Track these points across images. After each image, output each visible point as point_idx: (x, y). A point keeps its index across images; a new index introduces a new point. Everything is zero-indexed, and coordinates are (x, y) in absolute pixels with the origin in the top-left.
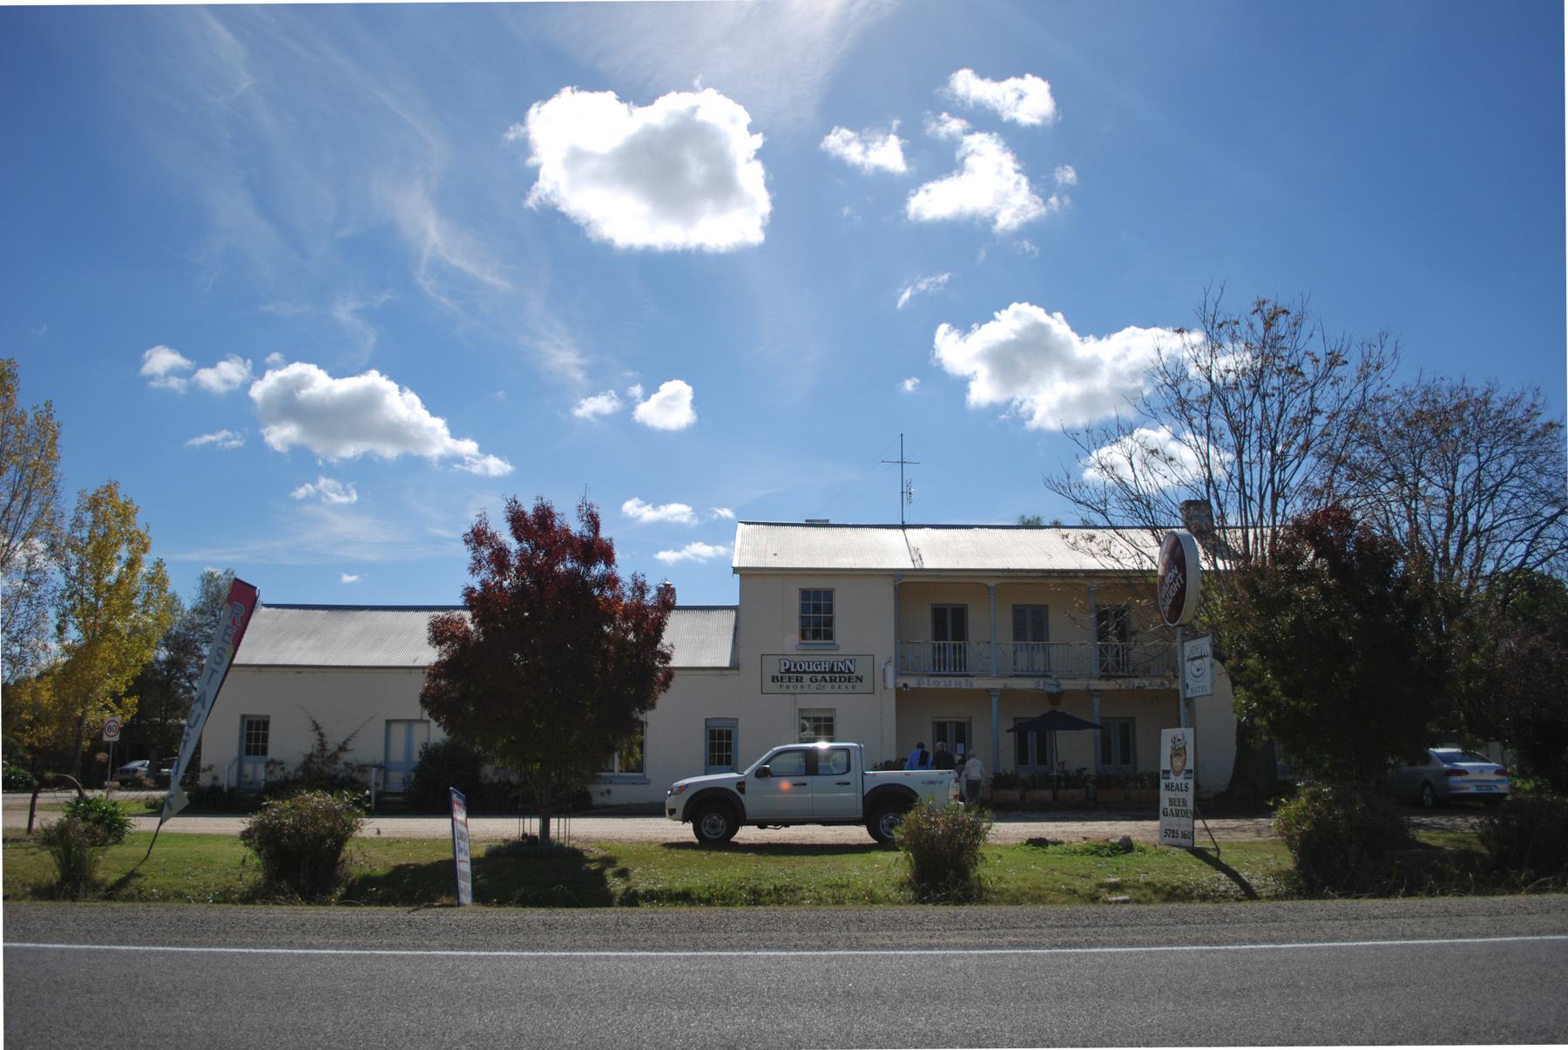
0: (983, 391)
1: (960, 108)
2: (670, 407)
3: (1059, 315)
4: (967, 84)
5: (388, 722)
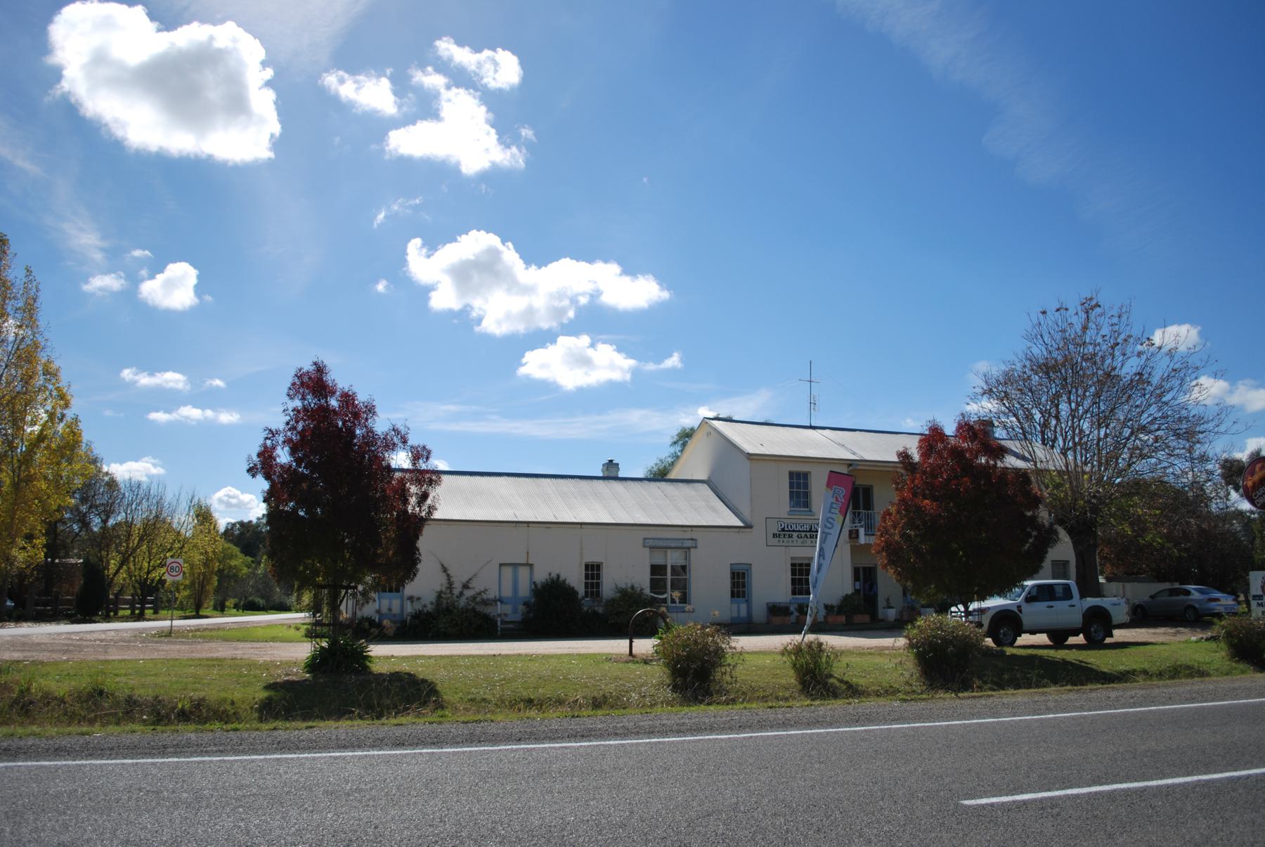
0: (444, 299)
1: (444, 67)
2: (175, 287)
3: (510, 244)
4: (447, 47)
5: (501, 565)
